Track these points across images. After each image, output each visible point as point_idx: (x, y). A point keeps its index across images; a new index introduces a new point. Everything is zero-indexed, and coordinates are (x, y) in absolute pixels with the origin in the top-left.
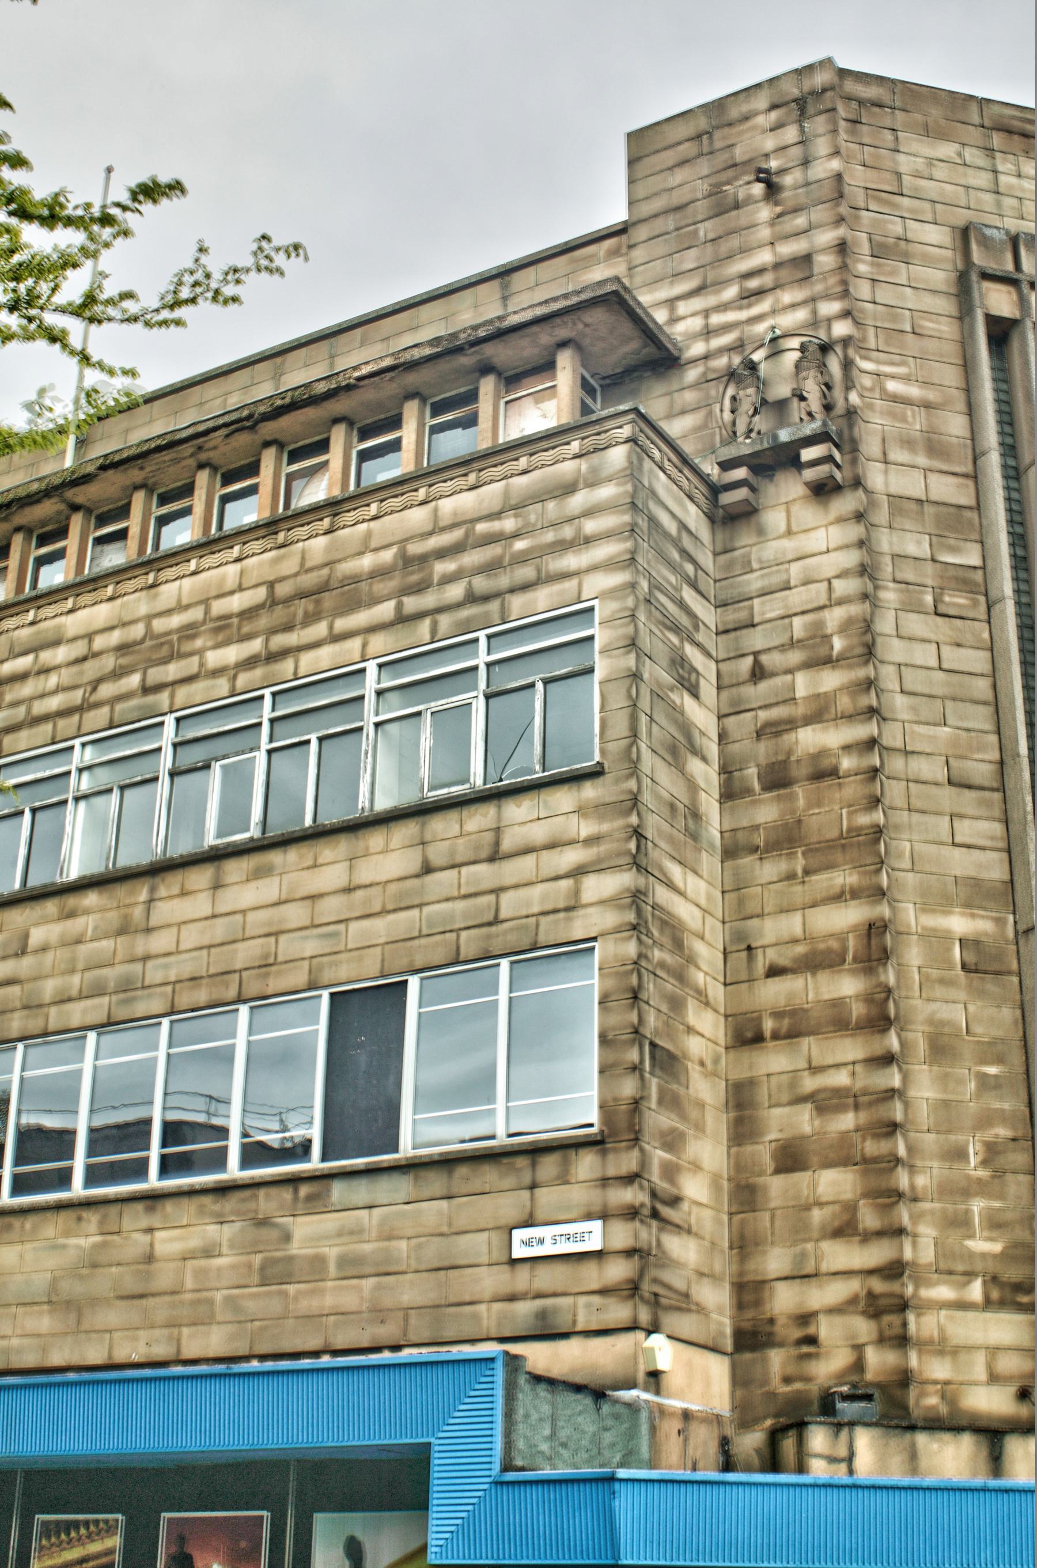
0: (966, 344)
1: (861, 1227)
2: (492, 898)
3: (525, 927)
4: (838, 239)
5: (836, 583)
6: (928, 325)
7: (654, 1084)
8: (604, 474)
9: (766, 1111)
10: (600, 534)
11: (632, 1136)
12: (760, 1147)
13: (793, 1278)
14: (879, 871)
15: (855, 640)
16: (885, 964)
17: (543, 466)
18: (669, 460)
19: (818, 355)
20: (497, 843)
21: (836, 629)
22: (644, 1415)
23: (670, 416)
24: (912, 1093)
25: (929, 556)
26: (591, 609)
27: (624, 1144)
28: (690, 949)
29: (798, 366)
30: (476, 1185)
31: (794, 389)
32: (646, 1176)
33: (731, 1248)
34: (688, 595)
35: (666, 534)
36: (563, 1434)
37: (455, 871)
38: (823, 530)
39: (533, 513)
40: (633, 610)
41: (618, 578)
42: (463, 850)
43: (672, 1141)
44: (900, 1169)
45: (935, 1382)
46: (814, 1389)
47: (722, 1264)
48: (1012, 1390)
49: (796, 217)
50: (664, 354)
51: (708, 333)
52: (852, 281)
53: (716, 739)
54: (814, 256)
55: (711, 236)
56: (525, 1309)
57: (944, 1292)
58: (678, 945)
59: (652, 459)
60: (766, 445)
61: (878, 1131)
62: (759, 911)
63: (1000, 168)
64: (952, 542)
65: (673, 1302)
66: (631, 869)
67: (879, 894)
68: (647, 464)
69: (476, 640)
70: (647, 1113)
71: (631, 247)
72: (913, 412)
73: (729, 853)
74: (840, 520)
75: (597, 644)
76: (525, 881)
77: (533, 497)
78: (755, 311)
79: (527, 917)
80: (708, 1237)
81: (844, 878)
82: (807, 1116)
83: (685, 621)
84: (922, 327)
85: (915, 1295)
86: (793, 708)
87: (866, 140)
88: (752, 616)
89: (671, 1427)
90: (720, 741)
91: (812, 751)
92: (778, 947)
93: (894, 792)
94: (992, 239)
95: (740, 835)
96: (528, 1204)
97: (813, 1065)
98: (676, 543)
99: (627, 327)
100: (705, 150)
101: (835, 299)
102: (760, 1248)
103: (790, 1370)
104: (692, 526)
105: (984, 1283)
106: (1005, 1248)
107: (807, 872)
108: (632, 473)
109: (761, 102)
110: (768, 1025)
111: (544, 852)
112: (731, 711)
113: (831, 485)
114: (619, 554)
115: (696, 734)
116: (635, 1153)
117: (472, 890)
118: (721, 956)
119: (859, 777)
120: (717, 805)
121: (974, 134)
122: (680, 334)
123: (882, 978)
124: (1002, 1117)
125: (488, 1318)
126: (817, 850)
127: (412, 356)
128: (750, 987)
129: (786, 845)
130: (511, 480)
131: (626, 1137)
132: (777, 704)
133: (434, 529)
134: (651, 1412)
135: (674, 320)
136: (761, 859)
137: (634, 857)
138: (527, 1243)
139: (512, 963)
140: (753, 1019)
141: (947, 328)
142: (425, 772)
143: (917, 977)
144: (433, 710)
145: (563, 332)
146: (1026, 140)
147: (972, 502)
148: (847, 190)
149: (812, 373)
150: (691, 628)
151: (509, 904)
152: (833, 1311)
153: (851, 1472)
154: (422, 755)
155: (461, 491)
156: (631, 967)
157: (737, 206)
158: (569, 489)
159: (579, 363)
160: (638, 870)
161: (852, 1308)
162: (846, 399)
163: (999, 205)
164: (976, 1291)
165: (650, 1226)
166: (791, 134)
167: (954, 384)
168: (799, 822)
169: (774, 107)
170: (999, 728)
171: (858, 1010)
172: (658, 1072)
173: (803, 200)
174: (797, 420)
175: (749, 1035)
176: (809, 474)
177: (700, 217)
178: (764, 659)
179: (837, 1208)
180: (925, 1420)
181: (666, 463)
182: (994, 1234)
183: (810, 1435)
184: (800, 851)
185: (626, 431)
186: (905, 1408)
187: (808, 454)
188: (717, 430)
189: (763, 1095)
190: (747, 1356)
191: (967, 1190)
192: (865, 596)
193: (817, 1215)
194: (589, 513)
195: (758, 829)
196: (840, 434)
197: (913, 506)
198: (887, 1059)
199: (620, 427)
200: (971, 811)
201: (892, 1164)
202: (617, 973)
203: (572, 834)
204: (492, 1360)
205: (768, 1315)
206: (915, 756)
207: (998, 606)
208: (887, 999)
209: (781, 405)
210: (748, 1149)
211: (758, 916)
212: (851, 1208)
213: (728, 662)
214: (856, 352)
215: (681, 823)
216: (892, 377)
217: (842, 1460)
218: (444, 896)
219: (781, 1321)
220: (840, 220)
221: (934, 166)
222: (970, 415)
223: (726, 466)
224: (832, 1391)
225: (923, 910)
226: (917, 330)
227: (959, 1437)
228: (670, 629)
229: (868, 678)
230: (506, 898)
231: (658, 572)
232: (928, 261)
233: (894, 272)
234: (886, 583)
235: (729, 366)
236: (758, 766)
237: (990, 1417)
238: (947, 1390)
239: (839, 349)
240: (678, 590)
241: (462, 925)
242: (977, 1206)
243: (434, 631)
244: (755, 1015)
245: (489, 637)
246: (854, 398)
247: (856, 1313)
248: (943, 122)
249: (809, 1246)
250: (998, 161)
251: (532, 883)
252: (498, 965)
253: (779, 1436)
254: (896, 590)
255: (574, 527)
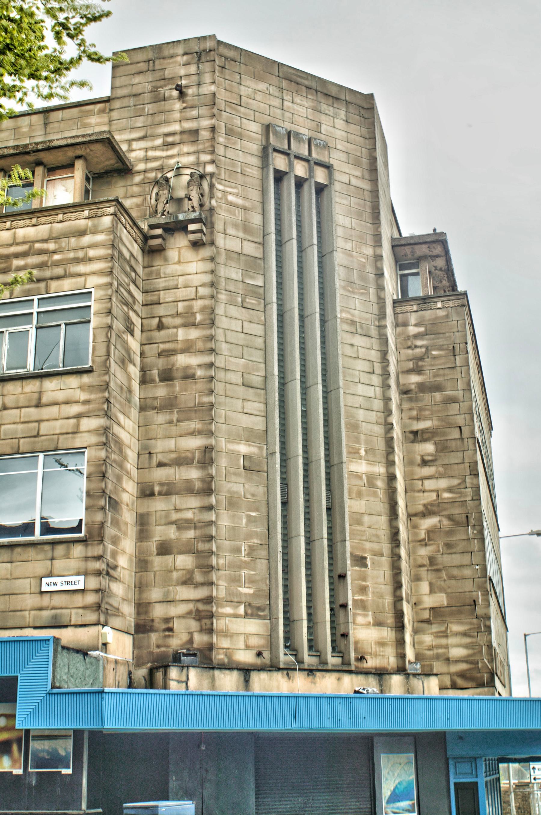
0: (264, 181)
1: (195, 581)
2: (36, 424)
3: (52, 440)
4: (212, 125)
5: (199, 288)
6: (248, 170)
7: (109, 514)
8: (100, 228)
9: (154, 527)
10: (96, 257)
11: (100, 539)
12: (151, 543)
13: (163, 602)
14: (211, 423)
15: (207, 317)
16: (211, 466)
17: (70, 220)
18: (128, 223)
19: (199, 179)
20: (40, 399)
21: (198, 311)
22: (101, 662)
23: (125, 197)
24: (220, 523)
25: (241, 280)
26: (91, 292)
27: (96, 542)
28: (125, 453)
29: (189, 183)
30: (25, 557)
31: (186, 194)
32: (105, 557)
33: (135, 588)
34: (132, 288)
35: (125, 259)
36: (72, 671)
37: (18, 410)
38: (195, 263)
39: (64, 242)
40: (111, 296)
41: (105, 280)
42: (22, 400)
43: (115, 541)
44: (213, 556)
45: (223, 649)
46: (170, 651)
47: (132, 595)
48: (254, 652)
49: (192, 111)
50: (125, 167)
51: (146, 160)
52: (217, 146)
53: (139, 355)
54: (200, 131)
55: (151, 112)
56: (46, 614)
57: (228, 610)
58: (121, 451)
59: (122, 223)
60: (172, 220)
61: (205, 539)
62: (155, 437)
63: (285, 98)
64: (251, 274)
65: (113, 612)
66: (104, 417)
67: (211, 434)
68: (120, 225)
69: (33, 300)
70: (106, 528)
71: (111, 110)
72: (239, 211)
73: (142, 409)
74: (203, 259)
75: (93, 310)
76: (52, 418)
77: (64, 235)
78: (170, 153)
79: (53, 435)
80: (127, 583)
81: (194, 425)
82: (173, 531)
83: (130, 300)
84: (246, 171)
85: (217, 610)
86: (176, 344)
87: (227, 77)
88: (160, 300)
89: (110, 667)
90: (141, 356)
91: (183, 366)
92: (163, 454)
93: (219, 387)
94: (280, 133)
95: (148, 400)
96: (50, 567)
97: (177, 508)
98: (129, 262)
99: (110, 154)
100: (150, 69)
101: (208, 153)
102: (149, 588)
103: (160, 642)
104: (135, 254)
105: (245, 606)
106: (255, 591)
107: (178, 421)
108: (113, 230)
109: (180, 50)
110: (157, 489)
111: (63, 405)
112: (147, 343)
113: (201, 242)
114: (105, 269)
115: (132, 353)
116: (101, 547)
117: (27, 420)
118: (137, 456)
119: (205, 380)
120: (138, 386)
121: (275, 80)
122: (133, 158)
123: (210, 472)
124: (257, 535)
125: (29, 617)
126: (183, 411)
127: (4, 152)
128: (149, 471)
129: (169, 408)
130: (53, 225)
131: (97, 539)
132: (169, 342)
133: (13, 243)
134: (104, 661)
135: (131, 150)
136: (157, 413)
137: (106, 412)
138: (48, 584)
139: (45, 455)
140: (150, 486)
141: (255, 172)
142: (5, 361)
143: (224, 471)
144: (10, 331)
145: (79, 152)
146: (297, 85)
147: (260, 256)
148: (217, 101)
149: (195, 188)
150: (132, 304)
151: (45, 428)
152: (179, 617)
153: (187, 688)
154: (3, 353)
155: (28, 226)
156: (102, 462)
157: (164, 99)
158: (82, 233)
159: (85, 167)
160: (107, 418)
161: (189, 616)
162: (210, 202)
163: (283, 115)
164: (241, 610)
165: (106, 579)
166: (193, 69)
167: (257, 200)
168: (176, 397)
169: (185, 54)
170: (265, 361)
171: (198, 485)
172: (111, 510)
173: (196, 103)
174: (187, 209)
175: (148, 492)
176: (192, 237)
177: (146, 102)
178: (164, 320)
179: (184, 572)
180: (218, 665)
181: (127, 225)
182: (250, 586)
183: (171, 671)
184: (175, 411)
185: (112, 210)
186: (211, 660)
187: (192, 227)
188: (148, 208)
189: (153, 520)
190: (141, 635)
191: (241, 566)
192: (212, 297)
193: (175, 575)
194: (92, 246)
195: (157, 399)
196: (206, 218)
197: (236, 256)
198: (210, 508)
199: (109, 207)
200: (251, 398)
201: (210, 554)
202: (96, 465)
203: (77, 398)
204: (49, 640)
205: (151, 618)
206: (229, 371)
207: (269, 306)
208: (212, 481)
209: (179, 201)
210: (145, 544)
211: (155, 439)
212: (191, 572)
213: (147, 319)
214: (216, 180)
215: (124, 396)
216: (231, 193)
217: (182, 682)
218: (12, 421)
219: (157, 621)
220: (213, 116)
221: (256, 93)
222: (263, 215)
223: (152, 227)
224: (179, 651)
225: (229, 442)
226: (243, 172)
227: (232, 672)
228: (124, 304)
229: (211, 335)
230: (43, 425)
231: (121, 277)
232: (251, 140)
233: (235, 143)
234: (222, 291)
235: (156, 178)
236: (158, 369)
237: (245, 664)
238: (228, 652)
239: (208, 178)
240: (128, 285)
241: (21, 436)
242: (244, 573)
243: (11, 294)
244: (150, 484)
245: (39, 299)
246: (214, 202)
247: (191, 618)
248: (261, 72)
249: (171, 588)
250: (284, 94)
251: (56, 419)
252: (38, 456)
253: (155, 671)
254: (225, 294)
255: (84, 252)
